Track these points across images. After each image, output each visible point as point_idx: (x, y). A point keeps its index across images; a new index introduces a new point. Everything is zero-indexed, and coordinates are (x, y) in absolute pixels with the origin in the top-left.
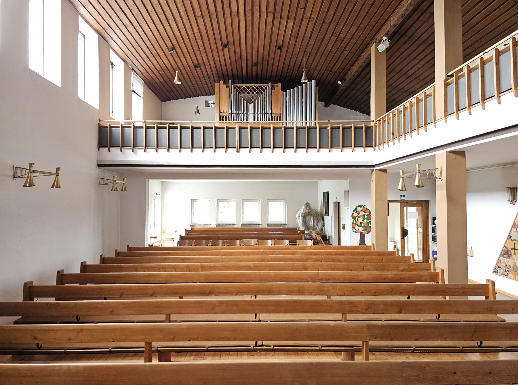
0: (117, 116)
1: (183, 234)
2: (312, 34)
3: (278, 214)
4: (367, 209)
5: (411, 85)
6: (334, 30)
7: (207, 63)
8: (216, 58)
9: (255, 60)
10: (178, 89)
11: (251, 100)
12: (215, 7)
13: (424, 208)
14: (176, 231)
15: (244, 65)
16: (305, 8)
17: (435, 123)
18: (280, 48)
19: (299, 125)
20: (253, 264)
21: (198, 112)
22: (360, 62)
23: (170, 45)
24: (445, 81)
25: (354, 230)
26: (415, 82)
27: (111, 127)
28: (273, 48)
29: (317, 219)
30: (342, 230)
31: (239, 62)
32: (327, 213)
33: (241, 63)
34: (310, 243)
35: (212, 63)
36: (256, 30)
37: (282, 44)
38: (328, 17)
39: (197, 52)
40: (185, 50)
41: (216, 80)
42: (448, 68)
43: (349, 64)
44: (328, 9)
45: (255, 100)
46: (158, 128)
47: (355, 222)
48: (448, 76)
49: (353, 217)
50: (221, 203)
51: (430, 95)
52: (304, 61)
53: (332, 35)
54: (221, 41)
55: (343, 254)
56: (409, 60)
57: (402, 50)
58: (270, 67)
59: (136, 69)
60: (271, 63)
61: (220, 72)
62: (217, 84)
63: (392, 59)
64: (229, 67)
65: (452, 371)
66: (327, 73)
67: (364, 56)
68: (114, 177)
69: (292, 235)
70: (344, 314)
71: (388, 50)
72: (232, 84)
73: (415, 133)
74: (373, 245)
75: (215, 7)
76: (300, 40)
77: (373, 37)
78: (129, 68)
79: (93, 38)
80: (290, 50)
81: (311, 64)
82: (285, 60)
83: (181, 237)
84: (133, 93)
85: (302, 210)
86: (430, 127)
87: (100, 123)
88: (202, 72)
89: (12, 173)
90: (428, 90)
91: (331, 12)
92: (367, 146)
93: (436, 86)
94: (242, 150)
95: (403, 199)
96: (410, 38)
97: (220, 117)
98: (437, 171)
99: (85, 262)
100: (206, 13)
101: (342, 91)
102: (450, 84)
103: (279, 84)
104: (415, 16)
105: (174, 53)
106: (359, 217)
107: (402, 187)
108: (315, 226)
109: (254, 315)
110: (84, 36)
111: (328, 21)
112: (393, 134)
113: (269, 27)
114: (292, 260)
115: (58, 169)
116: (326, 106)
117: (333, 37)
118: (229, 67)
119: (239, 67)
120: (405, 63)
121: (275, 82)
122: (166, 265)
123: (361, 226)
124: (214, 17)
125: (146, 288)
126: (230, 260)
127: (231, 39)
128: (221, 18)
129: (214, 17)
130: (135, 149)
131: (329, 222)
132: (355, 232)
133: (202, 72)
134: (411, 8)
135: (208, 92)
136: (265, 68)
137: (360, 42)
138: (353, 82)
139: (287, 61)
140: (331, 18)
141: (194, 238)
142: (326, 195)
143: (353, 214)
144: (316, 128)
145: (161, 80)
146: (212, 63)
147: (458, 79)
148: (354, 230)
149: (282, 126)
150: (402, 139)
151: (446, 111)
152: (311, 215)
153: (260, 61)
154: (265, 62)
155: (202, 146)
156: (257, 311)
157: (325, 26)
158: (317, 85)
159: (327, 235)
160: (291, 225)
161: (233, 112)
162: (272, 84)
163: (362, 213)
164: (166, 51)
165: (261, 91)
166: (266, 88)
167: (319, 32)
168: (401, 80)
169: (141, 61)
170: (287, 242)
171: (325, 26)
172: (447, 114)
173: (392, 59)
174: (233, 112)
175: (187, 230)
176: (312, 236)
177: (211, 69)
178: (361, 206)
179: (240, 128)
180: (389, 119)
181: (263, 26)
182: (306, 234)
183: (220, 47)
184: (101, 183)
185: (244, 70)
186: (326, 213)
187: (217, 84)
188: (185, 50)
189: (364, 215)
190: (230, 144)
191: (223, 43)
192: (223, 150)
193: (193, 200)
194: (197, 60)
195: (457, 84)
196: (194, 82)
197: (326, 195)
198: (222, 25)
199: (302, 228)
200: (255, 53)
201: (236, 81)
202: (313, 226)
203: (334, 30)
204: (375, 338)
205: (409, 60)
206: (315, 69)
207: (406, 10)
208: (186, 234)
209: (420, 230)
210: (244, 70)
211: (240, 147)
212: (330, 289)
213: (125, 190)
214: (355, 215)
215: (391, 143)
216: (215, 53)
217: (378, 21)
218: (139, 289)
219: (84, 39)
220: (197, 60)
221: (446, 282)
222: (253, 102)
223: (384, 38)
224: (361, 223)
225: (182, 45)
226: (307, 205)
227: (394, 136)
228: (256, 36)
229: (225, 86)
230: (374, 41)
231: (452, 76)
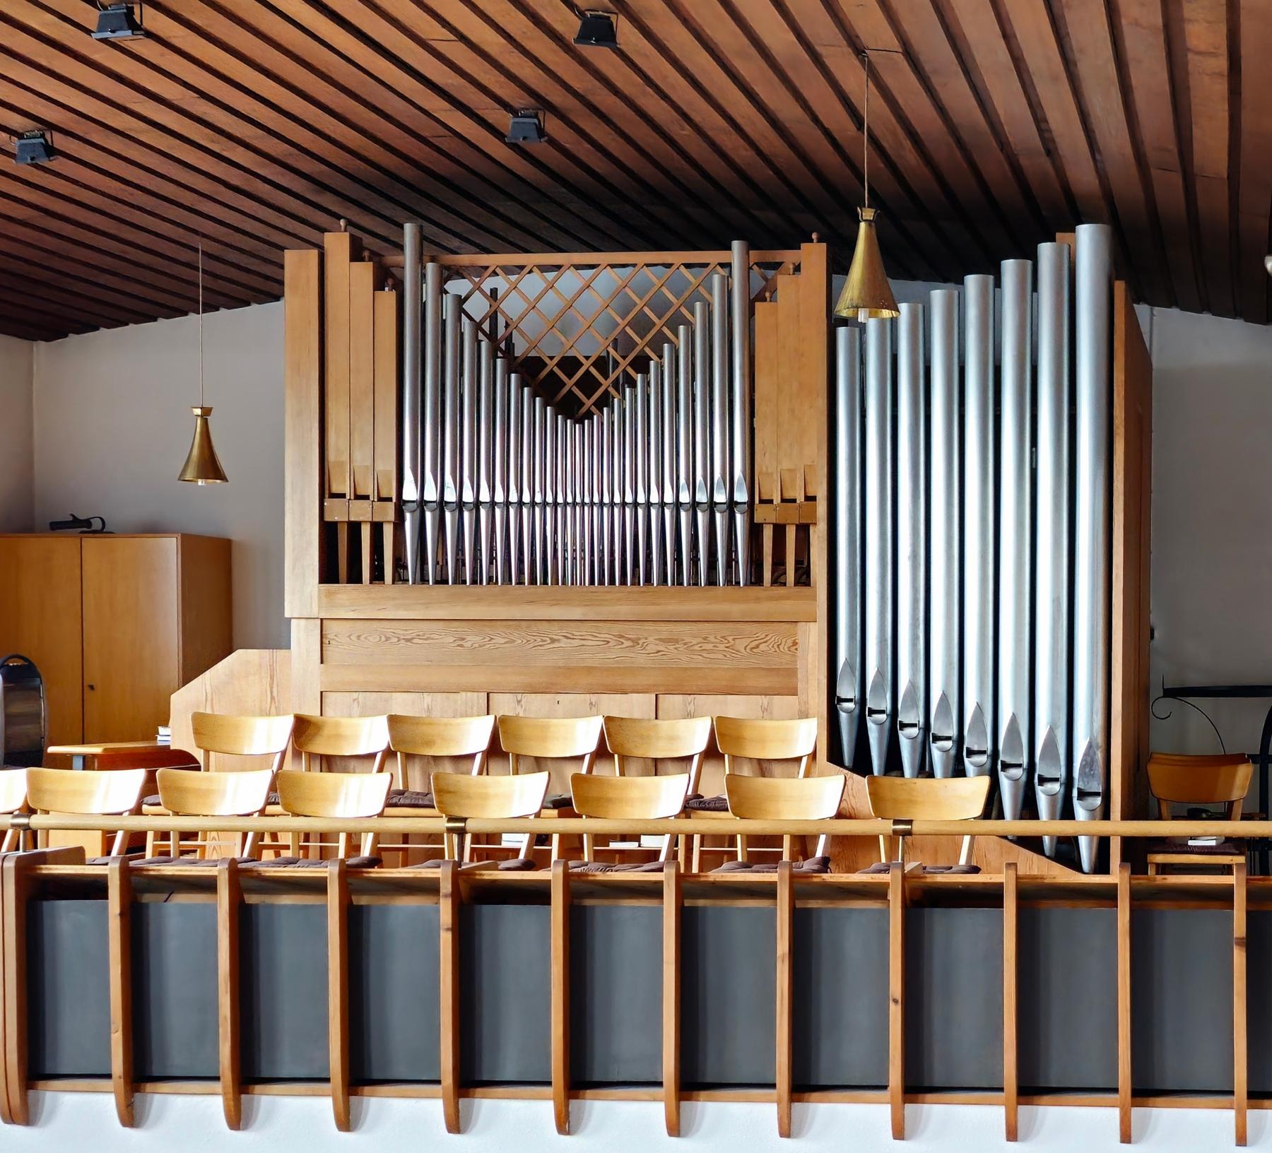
21: (210, 467)
72: (420, 261)
97: (328, 531)
229: (364, 271)
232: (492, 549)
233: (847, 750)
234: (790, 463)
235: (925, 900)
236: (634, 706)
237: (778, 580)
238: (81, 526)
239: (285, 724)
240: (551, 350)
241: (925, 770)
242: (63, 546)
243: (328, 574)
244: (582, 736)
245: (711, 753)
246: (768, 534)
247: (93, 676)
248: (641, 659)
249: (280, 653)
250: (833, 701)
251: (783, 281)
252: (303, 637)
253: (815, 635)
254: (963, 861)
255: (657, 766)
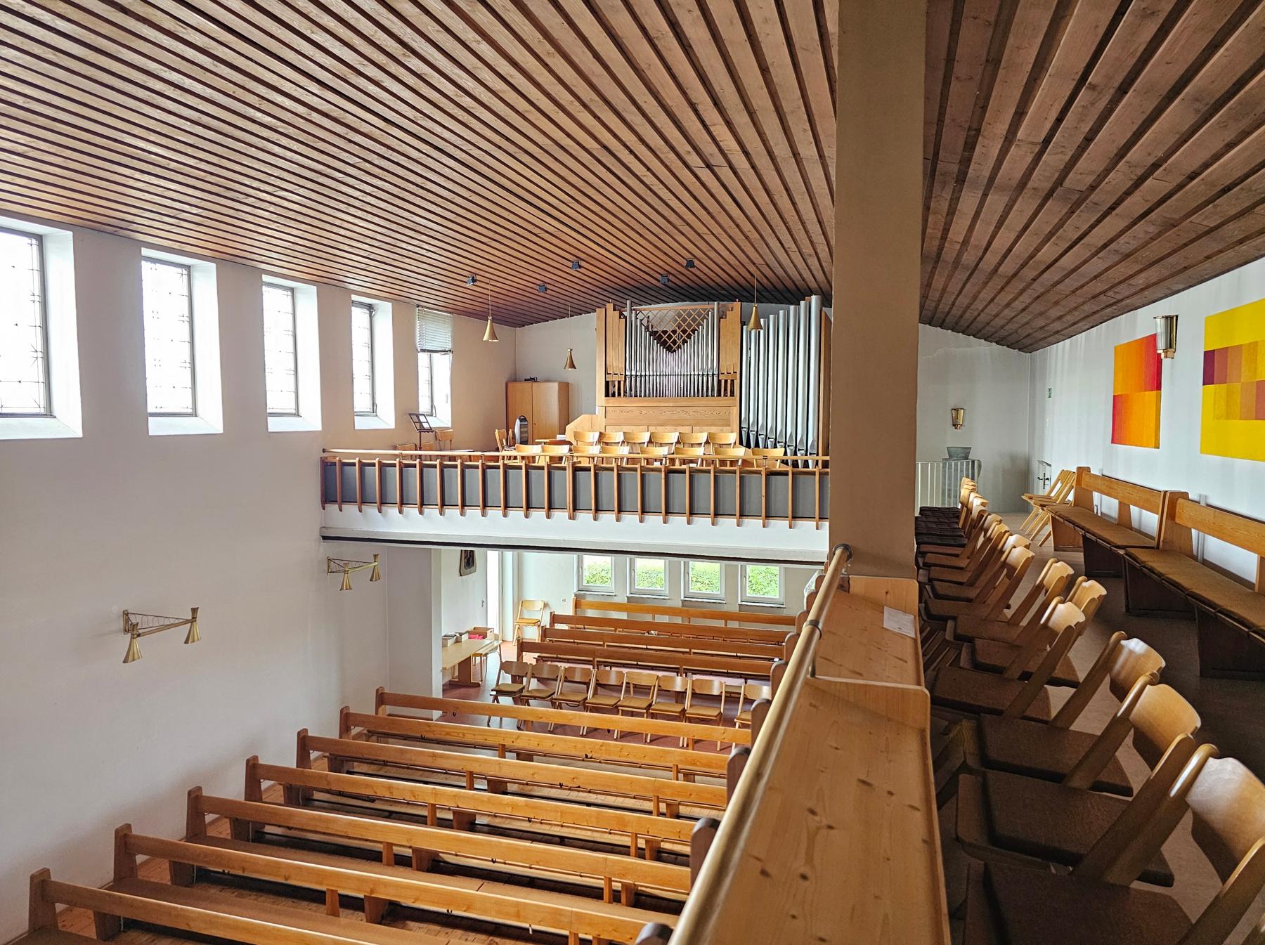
18: (690, 264)
21: (573, 366)
89: (121, 624)
97: (607, 383)
115: (194, 610)
130: (384, 508)
184: (333, 566)
233: (744, 441)
234: (729, 363)
235: (771, 474)
236: (686, 429)
237: (725, 395)
238: (533, 380)
239: (597, 435)
240: (660, 329)
241: (766, 447)
242: (529, 384)
243: (607, 395)
244: (673, 437)
245: (707, 442)
247: (535, 421)
248: (687, 416)
250: (741, 428)
252: (599, 411)
253: (736, 410)
255: (661, 445)
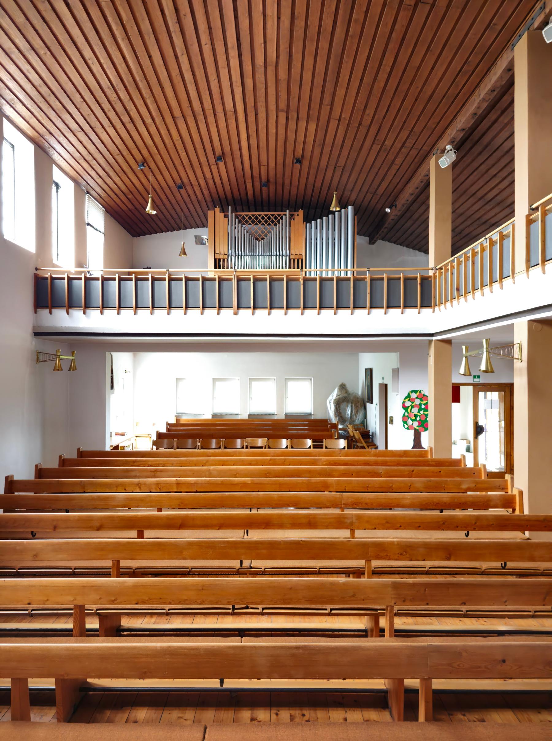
0: (63, 261)
1: (163, 430)
2: (344, 141)
3: (301, 398)
4: (424, 395)
5: (492, 213)
6: (376, 135)
7: (195, 183)
8: (208, 175)
9: (264, 178)
10: (155, 219)
11: (260, 235)
12: (202, 103)
13: (508, 393)
14: (154, 424)
15: (249, 185)
16: (332, 105)
17: (513, 277)
18: (299, 161)
19: (324, 276)
20: (252, 480)
21: (185, 253)
22: (416, 182)
23: (139, 158)
24: (528, 216)
25: (406, 426)
26: (497, 209)
27: (53, 279)
28: (289, 160)
29: (356, 407)
30: (389, 425)
31: (241, 181)
32: (371, 400)
33: (245, 182)
34: (342, 443)
35: (202, 182)
36: (263, 136)
37: (303, 156)
38: (365, 117)
39: (180, 168)
40: (161, 165)
41: (210, 206)
42: (532, 198)
43: (400, 184)
44: (366, 107)
45: (266, 236)
46: (120, 279)
47: (406, 414)
48: (533, 209)
49: (404, 406)
50: (217, 383)
51: (508, 236)
52: (336, 179)
53: (373, 143)
54: (214, 151)
55: (384, 464)
56: (486, 178)
57: (475, 164)
58: (287, 187)
59: (93, 192)
60: (287, 182)
61: (215, 195)
62: (210, 213)
63: (462, 177)
64: (227, 188)
65: (500, 658)
66: (369, 196)
67: (421, 172)
68: (57, 351)
69: (318, 429)
70: (368, 561)
71: (454, 165)
72: (232, 212)
73: (487, 289)
74: (431, 449)
75: (202, 103)
76: (327, 149)
77: (434, 146)
78: (81, 191)
79: (27, 150)
80: (315, 163)
81: (346, 184)
82: (307, 178)
83: (160, 435)
84: (88, 227)
85: (334, 395)
86: (507, 282)
87: (38, 272)
88: (189, 195)
90: (506, 228)
91: (370, 111)
92: (422, 306)
93: (515, 222)
94: (241, 312)
95: (477, 380)
96: (486, 146)
97: (215, 260)
98: (516, 348)
99: (12, 476)
100: (188, 113)
101: (389, 223)
102: (535, 221)
103: (301, 212)
104: (493, 116)
105: (146, 169)
106: (412, 407)
107: (465, 370)
108: (354, 417)
109: (239, 561)
110: (13, 146)
111: (367, 120)
112: (458, 290)
113: (281, 131)
114: (310, 473)
116: (372, 242)
117: (374, 145)
118: (227, 188)
119: (242, 187)
120: (481, 183)
121: (294, 208)
122: (126, 482)
123: (415, 420)
124: (201, 118)
125: (90, 519)
126: (221, 474)
127: (227, 149)
128: (211, 119)
129: (201, 118)
130: (88, 311)
131: (373, 411)
132: (408, 428)
133: (189, 195)
134: (485, 105)
135: (199, 222)
136: (279, 188)
137: (414, 152)
138: (408, 209)
139: (311, 179)
140: (370, 119)
141: (179, 435)
142: (369, 372)
143: (404, 403)
144: (349, 279)
145: (130, 206)
146: (202, 182)
147: (545, 214)
148: (406, 426)
149: (301, 276)
150: (470, 296)
151: (528, 260)
152: (348, 402)
153: (272, 179)
154: (280, 181)
155: (184, 306)
156: (243, 557)
157: (363, 130)
158: (356, 213)
159: (369, 431)
160: (319, 416)
161: (233, 254)
162: (290, 211)
163: (417, 402)
164: (134, 166)
165: (275, 221)
166: (282, 218)
167: (355, 138)
168: (476, 207)
169: (99, 181)
170: (309, 442)
171: (363, 130)
172: (529, 265)
173: (462, 177)
174: (233, 254)
175: (170, 422)
176: (348, 432)
177: (201, 190)
178: (415, 392)
179: (239, 280)
180: (453, 267)
181: (272, 131)
182: (341, 429)
183: (212, 160)
184: (39, 358)
185: (250, 192)
186: (369, 399)
187: (210, 213)
188: (161, 165)
189: (420, 404)
190: (224, 304)
191: (217, 154)
192: (215, 311)
193: (178, 379)
194: (181, 178)
195: (543, 222)
196: (178, 210)
197: (369, 373)
198: (213, 130)
199: (334, 420)
200: (264, 169)
201: (239, 207)
202: (351, 417)
203: (376, 135)
204: (404, 601)
205: (486, 178)
206: (352, 190)
207: (478, 108)
208: (168, 430)
209: (503, 423)
210: (250, 192)
211: (239, 307)
212: (354, 521)
213: (75, 369)
214: (408, 404)
215: (455, 302)
216: (206, 169)
217: (438, 123)
218: (80, 519)
219: (14, 150)
220: (181, 178)
221: (526, 512)
222: (262, 239)
223: (449, 147)
224: (416, 416)
225: (158, 158)
226: (343, 387)
227: (460, 292)
228: (263, 143)
229: (222, 214)
230: (435, 151)
231: (537, 209)
232: (235, 264)
246: (292, 260)
249: (381, 382)
251: (296, 217)
254: (483, 367)
